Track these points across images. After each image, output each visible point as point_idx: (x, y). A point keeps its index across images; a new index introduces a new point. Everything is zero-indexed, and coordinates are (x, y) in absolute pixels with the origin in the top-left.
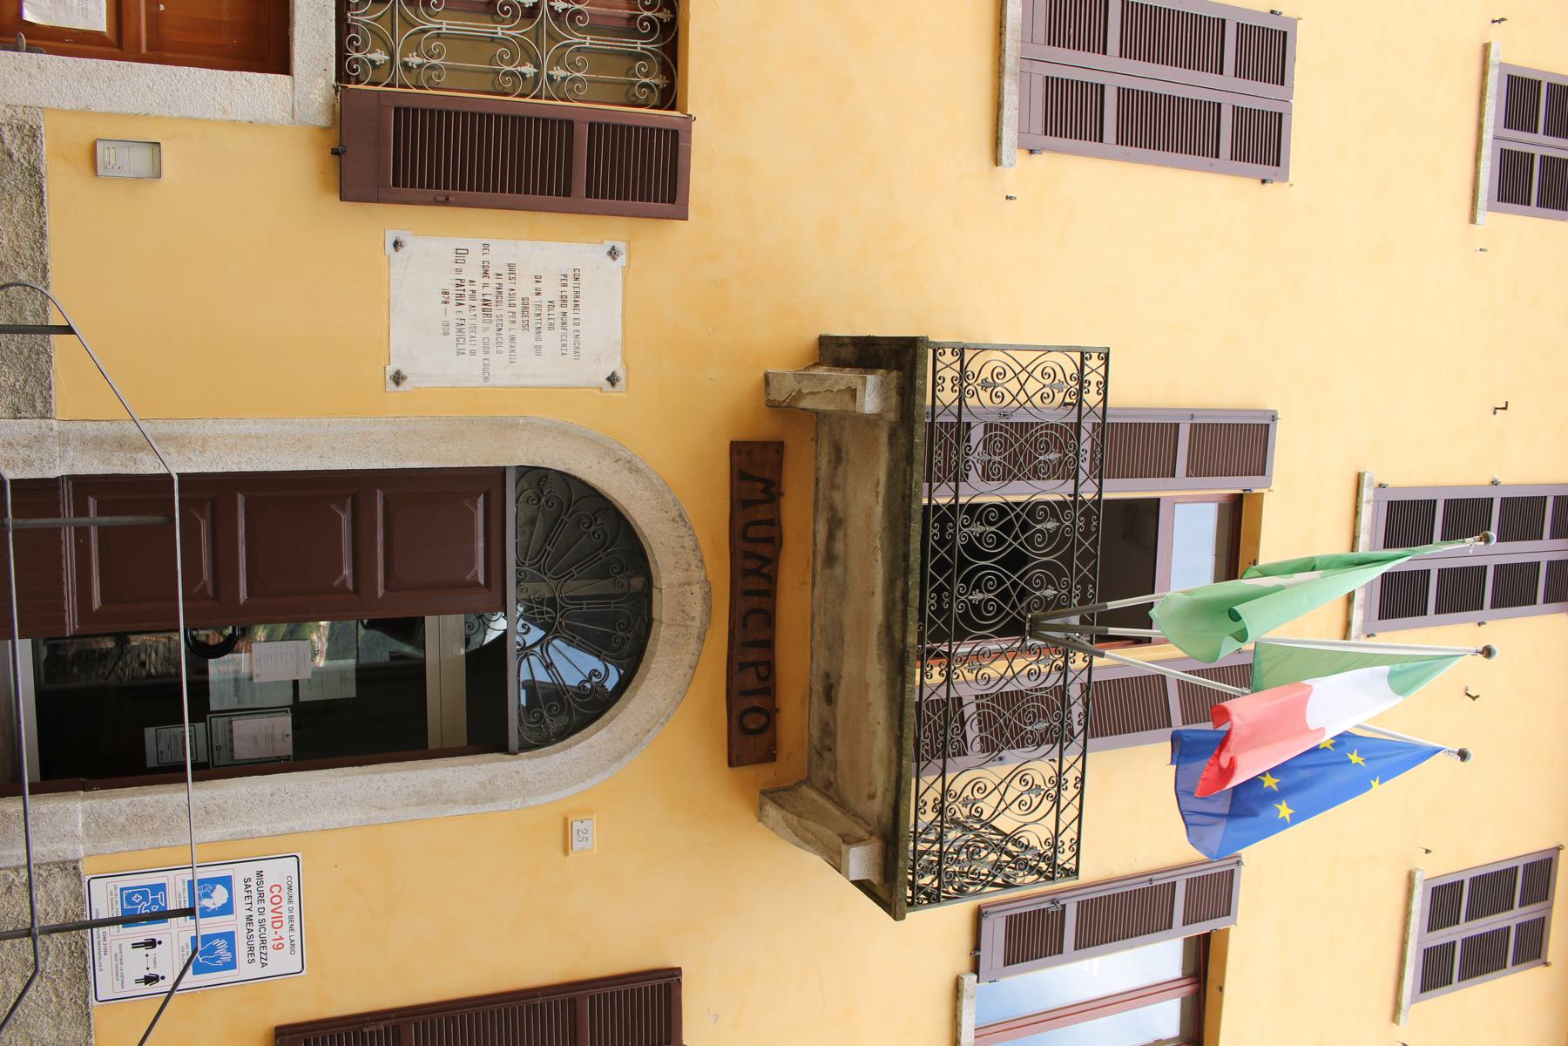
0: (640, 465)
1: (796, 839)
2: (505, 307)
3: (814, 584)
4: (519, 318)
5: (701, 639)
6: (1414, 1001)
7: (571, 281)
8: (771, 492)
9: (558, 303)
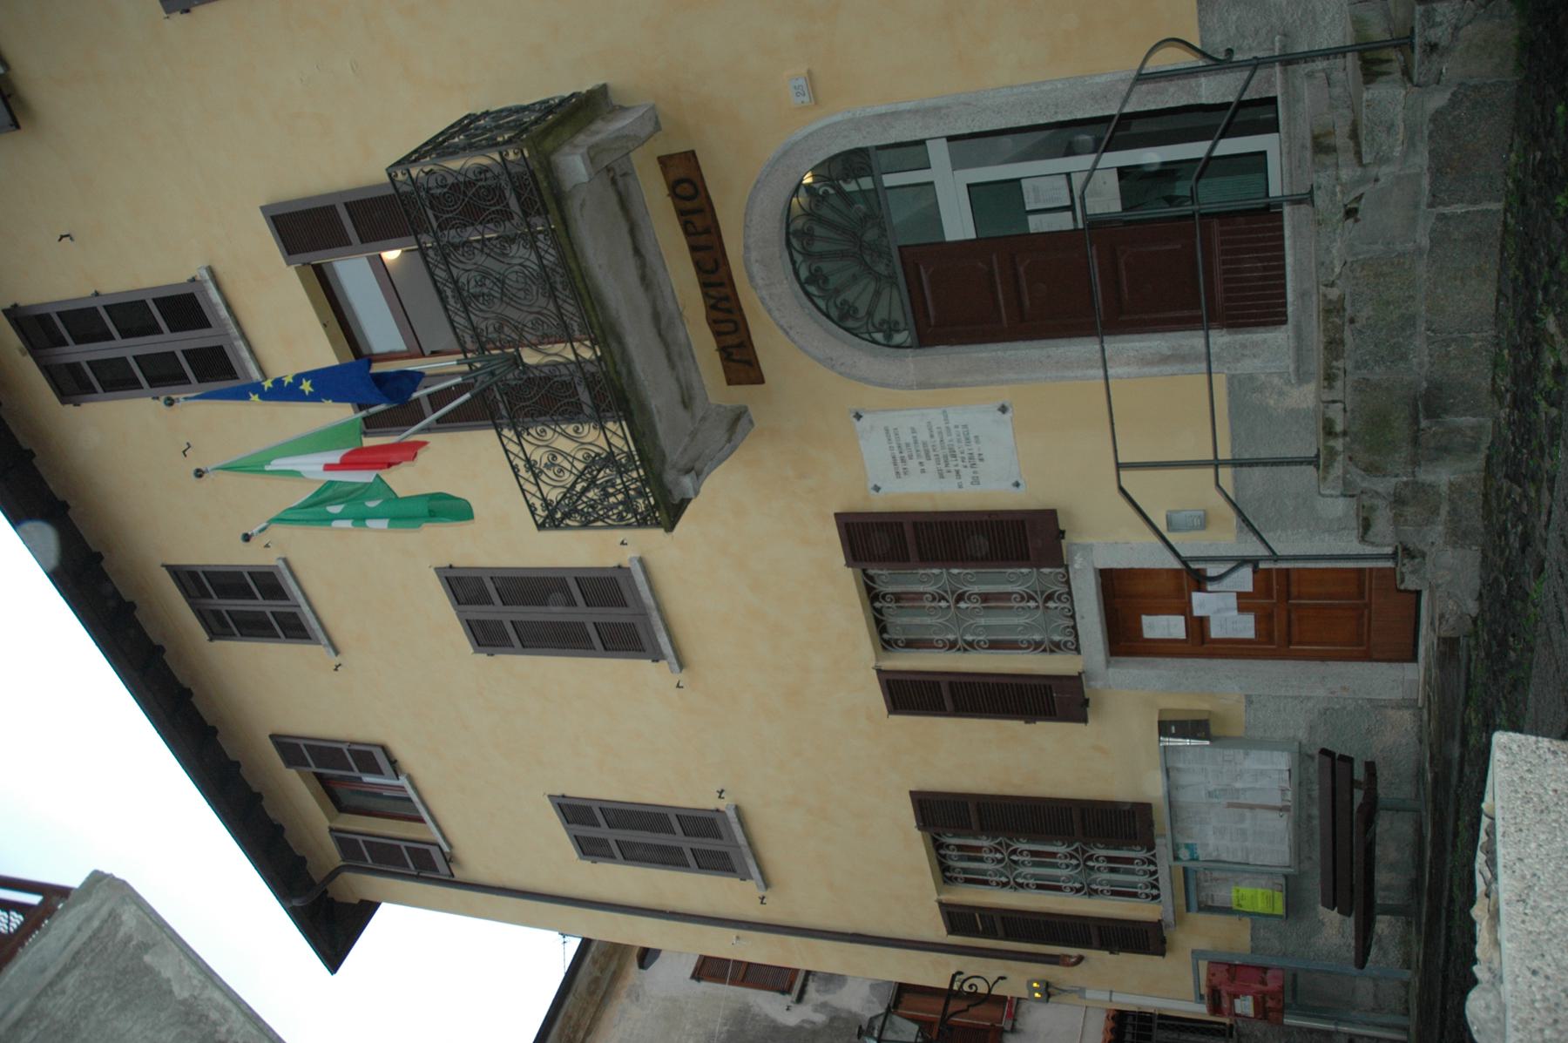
2: (941, 453)
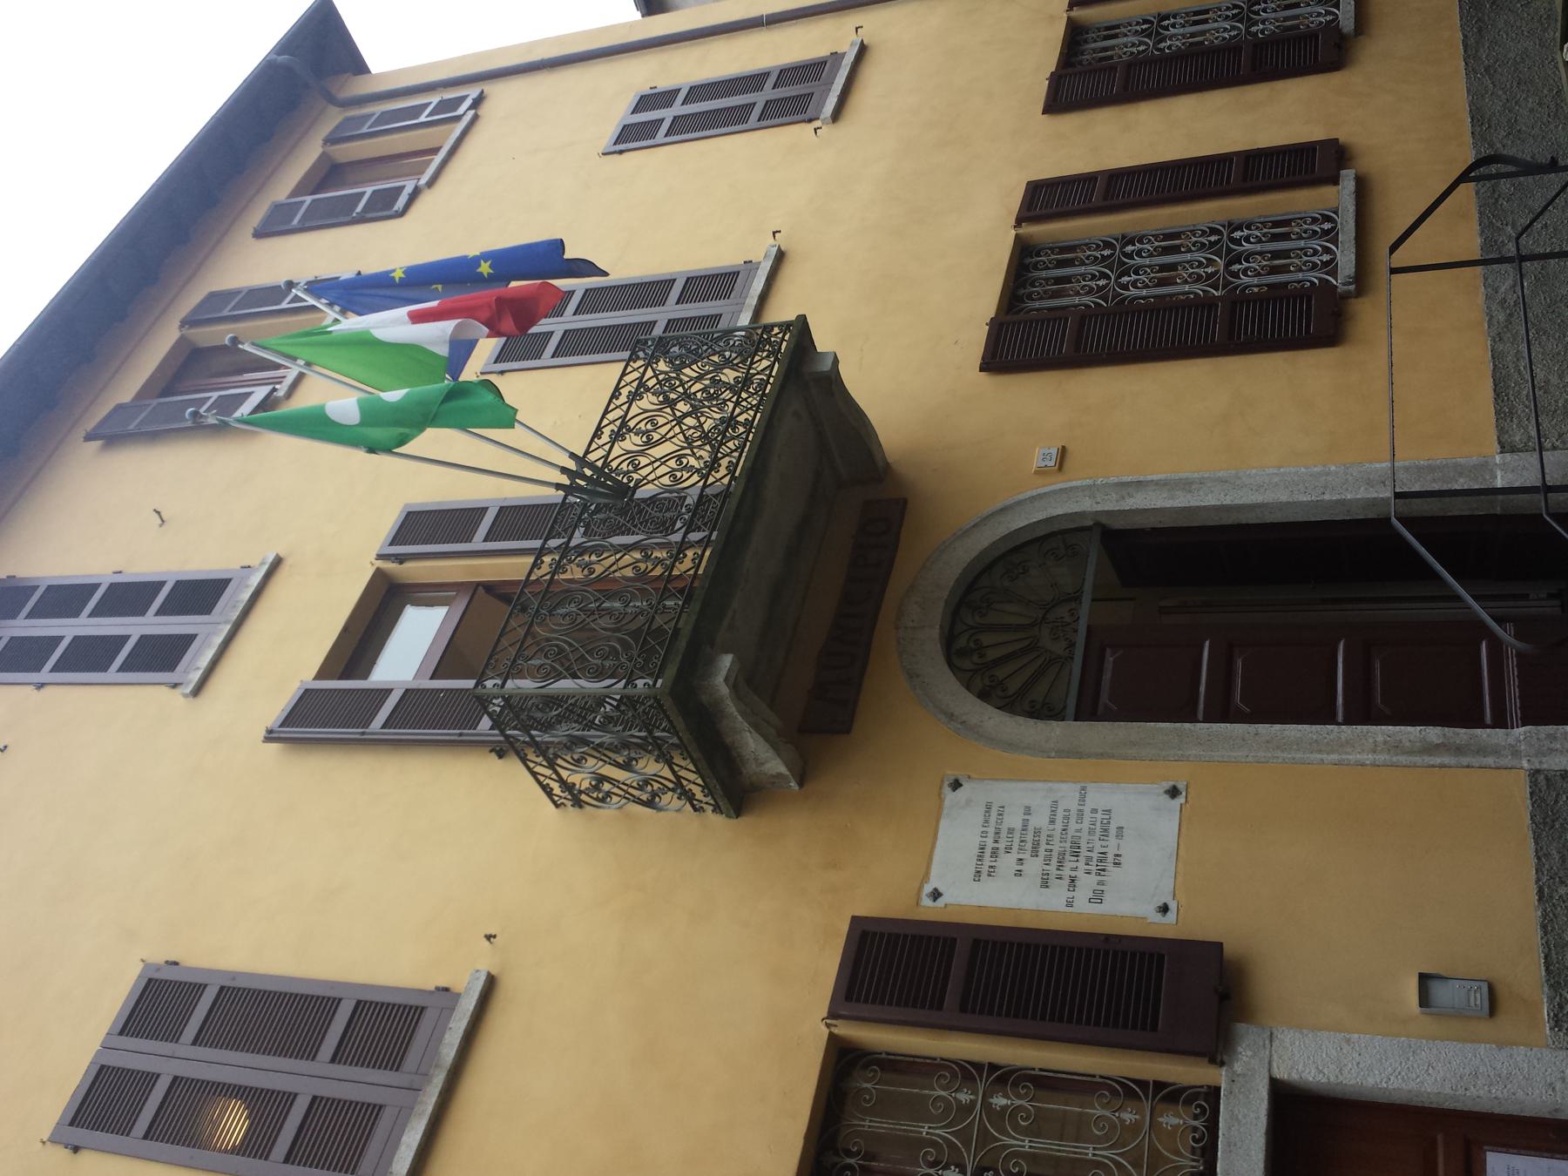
2: (1056, 848)
7: (985, 869)
9: (1002, 851)
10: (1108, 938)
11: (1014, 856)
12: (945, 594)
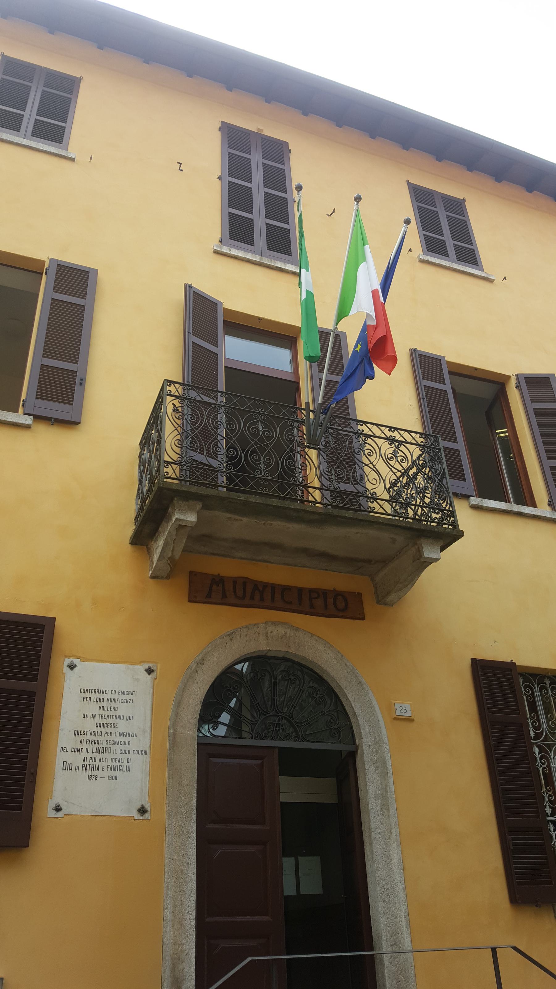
0: (200, 657)
1: (409, 586)
2: (102, 738)
3: (268, 562)
4: (109, 730)
5: (297, 629)
6: (482, 270)
7: (88, 695)
8: (218, 581)
9: (101, 704)
10: (34, 775)
11: (97, 712)
12: (292, 650)
